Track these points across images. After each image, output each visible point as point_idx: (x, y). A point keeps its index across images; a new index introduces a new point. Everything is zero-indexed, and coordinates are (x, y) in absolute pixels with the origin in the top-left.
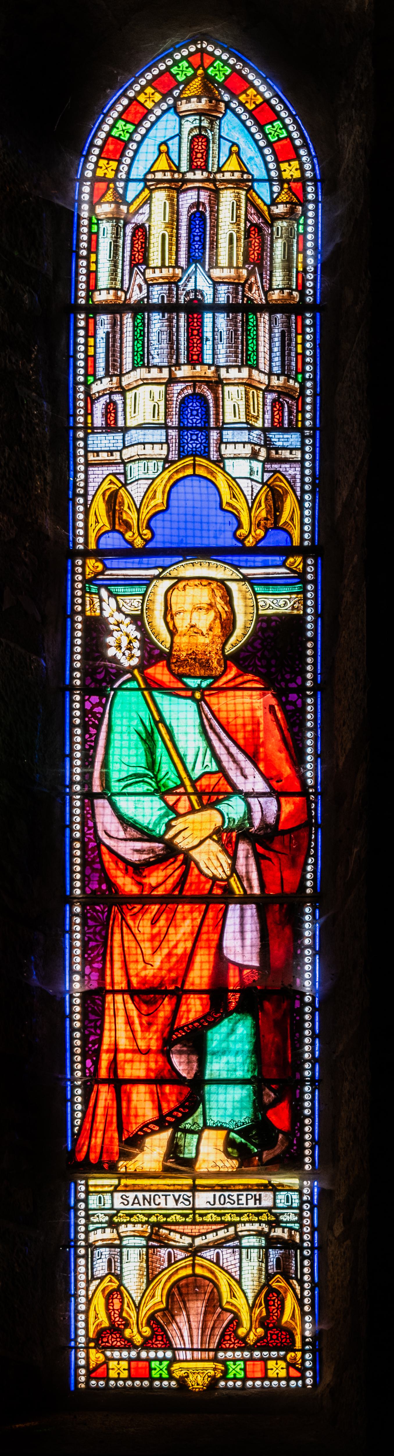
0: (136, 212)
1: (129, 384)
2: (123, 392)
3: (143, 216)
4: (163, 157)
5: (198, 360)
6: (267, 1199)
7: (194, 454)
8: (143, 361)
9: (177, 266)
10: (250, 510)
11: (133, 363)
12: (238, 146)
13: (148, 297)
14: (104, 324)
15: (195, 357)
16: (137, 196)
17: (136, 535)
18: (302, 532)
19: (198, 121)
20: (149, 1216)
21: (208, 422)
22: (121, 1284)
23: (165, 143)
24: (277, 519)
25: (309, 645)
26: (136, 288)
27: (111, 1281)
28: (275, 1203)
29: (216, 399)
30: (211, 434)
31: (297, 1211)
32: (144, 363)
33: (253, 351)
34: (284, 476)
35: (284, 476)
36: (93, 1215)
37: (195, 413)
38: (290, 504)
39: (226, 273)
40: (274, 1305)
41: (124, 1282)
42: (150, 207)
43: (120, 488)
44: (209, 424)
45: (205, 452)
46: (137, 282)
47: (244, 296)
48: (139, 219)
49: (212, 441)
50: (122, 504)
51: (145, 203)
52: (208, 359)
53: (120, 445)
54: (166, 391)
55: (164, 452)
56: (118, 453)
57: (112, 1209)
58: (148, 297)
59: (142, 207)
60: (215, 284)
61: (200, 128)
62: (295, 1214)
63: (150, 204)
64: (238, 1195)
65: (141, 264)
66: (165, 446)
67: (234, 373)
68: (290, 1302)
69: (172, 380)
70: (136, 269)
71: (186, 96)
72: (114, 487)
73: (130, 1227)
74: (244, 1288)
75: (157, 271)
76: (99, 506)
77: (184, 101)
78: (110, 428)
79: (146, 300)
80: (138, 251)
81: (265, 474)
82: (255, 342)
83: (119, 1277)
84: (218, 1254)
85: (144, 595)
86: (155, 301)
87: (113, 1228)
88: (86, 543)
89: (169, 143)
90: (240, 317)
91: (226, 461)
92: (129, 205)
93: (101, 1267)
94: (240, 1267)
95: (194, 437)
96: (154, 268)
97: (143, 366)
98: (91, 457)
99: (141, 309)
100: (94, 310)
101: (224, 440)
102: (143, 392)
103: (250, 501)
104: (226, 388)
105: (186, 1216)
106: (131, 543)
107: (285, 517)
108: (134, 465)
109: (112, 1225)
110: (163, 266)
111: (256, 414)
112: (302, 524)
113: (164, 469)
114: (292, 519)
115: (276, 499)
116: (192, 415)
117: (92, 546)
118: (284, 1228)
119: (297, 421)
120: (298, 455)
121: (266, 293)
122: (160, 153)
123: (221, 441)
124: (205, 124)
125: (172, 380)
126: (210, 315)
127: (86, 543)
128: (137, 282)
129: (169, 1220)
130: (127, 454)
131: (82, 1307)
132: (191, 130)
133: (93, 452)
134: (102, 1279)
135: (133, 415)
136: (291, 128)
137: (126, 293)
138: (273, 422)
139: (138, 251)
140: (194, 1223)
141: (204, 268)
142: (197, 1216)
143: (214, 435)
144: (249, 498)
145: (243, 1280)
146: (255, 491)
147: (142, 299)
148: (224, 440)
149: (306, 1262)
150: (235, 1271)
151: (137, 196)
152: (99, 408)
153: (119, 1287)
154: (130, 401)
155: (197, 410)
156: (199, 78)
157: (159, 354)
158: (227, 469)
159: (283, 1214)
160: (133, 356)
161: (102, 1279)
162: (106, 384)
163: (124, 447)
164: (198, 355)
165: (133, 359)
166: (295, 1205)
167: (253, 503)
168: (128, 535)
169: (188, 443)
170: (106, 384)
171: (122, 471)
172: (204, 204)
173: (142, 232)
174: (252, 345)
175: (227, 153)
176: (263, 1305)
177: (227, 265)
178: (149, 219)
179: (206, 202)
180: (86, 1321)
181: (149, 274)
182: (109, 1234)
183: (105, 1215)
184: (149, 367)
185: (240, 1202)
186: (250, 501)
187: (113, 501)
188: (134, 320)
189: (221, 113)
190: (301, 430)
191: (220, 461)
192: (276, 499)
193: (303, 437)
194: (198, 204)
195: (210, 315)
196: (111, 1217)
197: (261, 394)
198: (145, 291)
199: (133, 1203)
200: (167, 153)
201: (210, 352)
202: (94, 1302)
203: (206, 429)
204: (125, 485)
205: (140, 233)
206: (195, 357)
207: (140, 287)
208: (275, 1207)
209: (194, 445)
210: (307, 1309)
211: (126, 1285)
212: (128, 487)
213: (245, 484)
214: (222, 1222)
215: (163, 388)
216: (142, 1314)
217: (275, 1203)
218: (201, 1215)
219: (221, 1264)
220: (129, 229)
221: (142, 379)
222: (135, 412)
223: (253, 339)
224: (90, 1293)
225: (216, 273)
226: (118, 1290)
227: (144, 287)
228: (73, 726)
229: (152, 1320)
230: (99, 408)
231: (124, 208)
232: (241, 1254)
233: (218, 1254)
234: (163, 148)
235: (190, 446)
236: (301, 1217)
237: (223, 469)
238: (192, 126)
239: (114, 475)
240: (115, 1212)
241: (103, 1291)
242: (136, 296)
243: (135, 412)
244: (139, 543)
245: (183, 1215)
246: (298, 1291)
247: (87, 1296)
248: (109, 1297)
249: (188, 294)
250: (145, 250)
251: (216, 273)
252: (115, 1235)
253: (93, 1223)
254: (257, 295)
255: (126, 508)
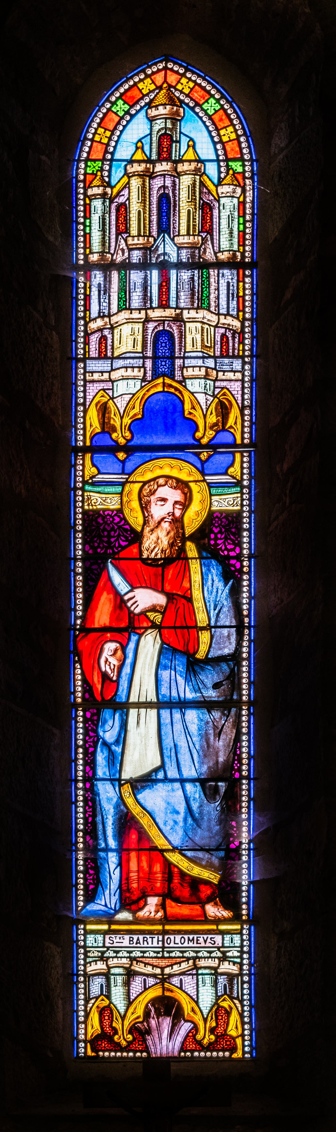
0: (118, 194)
1: (117, 323)
2: (112, 328)
3: (122, 197)
4: (140, 151)
5: (166, 304)
6: (218, 939)
7: (164, 375)
8: (125, 305)
9: (150, 235)
10: (205, 416)
11: (118, 307)
12: (194, 143)
13: (129, 258)
14: (98, 277)
15: (164, 302)
16: (119, 182)
17: (120, 435)
18: (243, 433)
19: (164, 124)
20: (130, 952)
21: (174, 352)
22: (111, 1003)
23: (140, 141)
24: (224, 424)
25: (244, 906)
26: (120, 252)
27: (103, 1000)
28: (223, 943)
29: (180, 332)
30: (176, 361)
31: (239, 949)
32: (126, 307)
33: (207, 297)
34: (230, 392)
35: (230, 392)
36: (89, 951)
37: (163, 345)
38: (234, 413)
39: (186, 240)
40: (222, 1019)
41: (113, 1001)
42: (129, 190)
43: (109, 400)
44: (175, 354)
45: (171, 375)
46: (121, 247)
47: (200, 257)
48: (122, 200)
49: (176, 367)
50: (110, 413)
51: (125, 187)
52: (173, 304)
53: (109, 369)
54: (143, 327)
55: (141, 374)
56: (108, 374)
57: (104, 946)
58: (129, 258)
59: (122, 190)
60: (179, 248)
61: (166, 128)
62: (238, 951)
63: (129, 188)
64: (197, 937)
65: (124, 233)
66: (142, 370)
67: (193, 314)
68: (234, 1017)
69: (148, 320)
70: (120, 237)
71: (154, 104)
72: (105, 400)
73: (115, 960)
74: (201, 1006)
75: (136, 238)
76: (93, 414)
77: (153, 109)
78: (102, 356)
79: (127, 261)
80: (122, 223)
81: (216, 390)
82: (208, 290)
83: (109, 997)
84: (181, 980)
85: (121, 494)
86: (134, 261)
87: (104, 961)
88: (84, 441)
89: (143, 141)
90: (196, 275)
91: (187, 380)
92: (112, 188)
93: (95, 989)
94: (198, 991)
95: (163, 363)
96: (133, 237)
97: (126, 309)
98: (88, 377)
99: (126, 266)
100: (88, 268)
101: (186, 365)
102: (126, 329)
103: (205, 411)
104: (188, 325)
105: (158, 952)
106: (116, 442)
107: (231, 422)
108: (120, 383)
109: (102, 958)
110: (139, 235)
111: (209, 345)
112: (243, 426)
113: (142, 387)
114: (236, 423)
115: (223, 410)
116: (162, 346)
117: (88, 443)
118: (229, 961)
119: (239, 350)
120: (239, 376)
121: (215, 254)
122: (137, 148)
123: (183, 368)
124: (169, 125)
125: (148, 320)
126: (175, 271)
127: (84, 441)
128: (121, 247)
129: (146, 955)
130: (115, 375)
131: (82, 1019)
132: (160, 130)
133: (89, 372)
134: (97, 998)
135: (119, 346)
136: (193, 78)
137: (113, 255)
138: (221, 351)
139: (122, 223)
140: (163, 957)
141: (170, 237)
142: (165, 952)
143: (178, 362)
144: (204, 407)
145: (200, 1000)
146: (209, 402)
147: (125, 260)
148: (186, 365)
149: (246, 986)
150: (193, 993)
151: (119, 182)
152: (94, 339)
153: (109, 1004)
154: (117, 337)
155: (166, 343)
156: (165, 91)
157: (136, 300)
158: (188, 386)
159: (229, 951)
160: (119, 301)
161: (97, 998)
162: (99, 323)
163: (112, 370)
164: (166, 301)
165: (119, 305)
166: (238, 945)
167: (207, 411)
168: (114, 435)
169: (159, 368)
170: (99, 323)
171: (111, 388)
172: (168, 187)
173: (123, 210)
174: (206, 292)
175: (186, 147)
176: (214, 1019)
177: (186, 234)
178: (128, 199)
179: (169, 185)
180: (86, 1029)
181: (130, 241)
182: (101, 966)
183: (98, 951)
184: (131, 310)
185: (199, 942)
186: (205, 411)
187: (104, 410)
188: (119, 274)
189: (180, 116)
190: (243, 357)
191: (182, 382)
192: (223, 410)
193: (244, 363)
194: (164, 187)
195: (175, 271)
196: (103, 953)
197: (212, 329)
198: (126, 254)
199: (137, 943)
200: (142, 148)
201: (175, 299)
202: (91, 1015)
203: (172, 358)
204: (112, 398)
205: (123, 209)
206: (164, 302)
207: (123, 251)
208: (223, 946)
209: (163, 369)
210: (246, 1020)
211: (115, 1003)
212: (115, 400)
213: (201, 398)
214: (183, 957)
215: (140, 326)
216: (127, 1023)
217: (223, 943)
218: (169, 952)
219: (184, 989)
220: (114, 206)
221: (127, 319)
222: (120, 344)
223: (206, 287)
224: (88, 1009)
225: (179, 240)
226: (109, 1006)
227: (126, 251)
228: (76, 574)
229: (132, 1030)
230: (94, 339)
231: (108, 190)
232: (197, 980)
233: (181, 980)
234: (139, 144)
235: (160, 370)
236: (242, 952)
237: (185, 387)
238: (160, 127)
239: (104, 390)
240: (105, 949)
241: (98, 1007)
242: (119, 258)
243: (120, 344)
244: (122, 441)
245: (154, 952)
246: (240, 1009)
247: (85, 1010)
248: (102, 1012)
249: (159, 256)
250: (127, 221)
251: (179, 240)
252: (105, 967)
253: (90, 957)
254: (210, 256)
255: (112, 416)
